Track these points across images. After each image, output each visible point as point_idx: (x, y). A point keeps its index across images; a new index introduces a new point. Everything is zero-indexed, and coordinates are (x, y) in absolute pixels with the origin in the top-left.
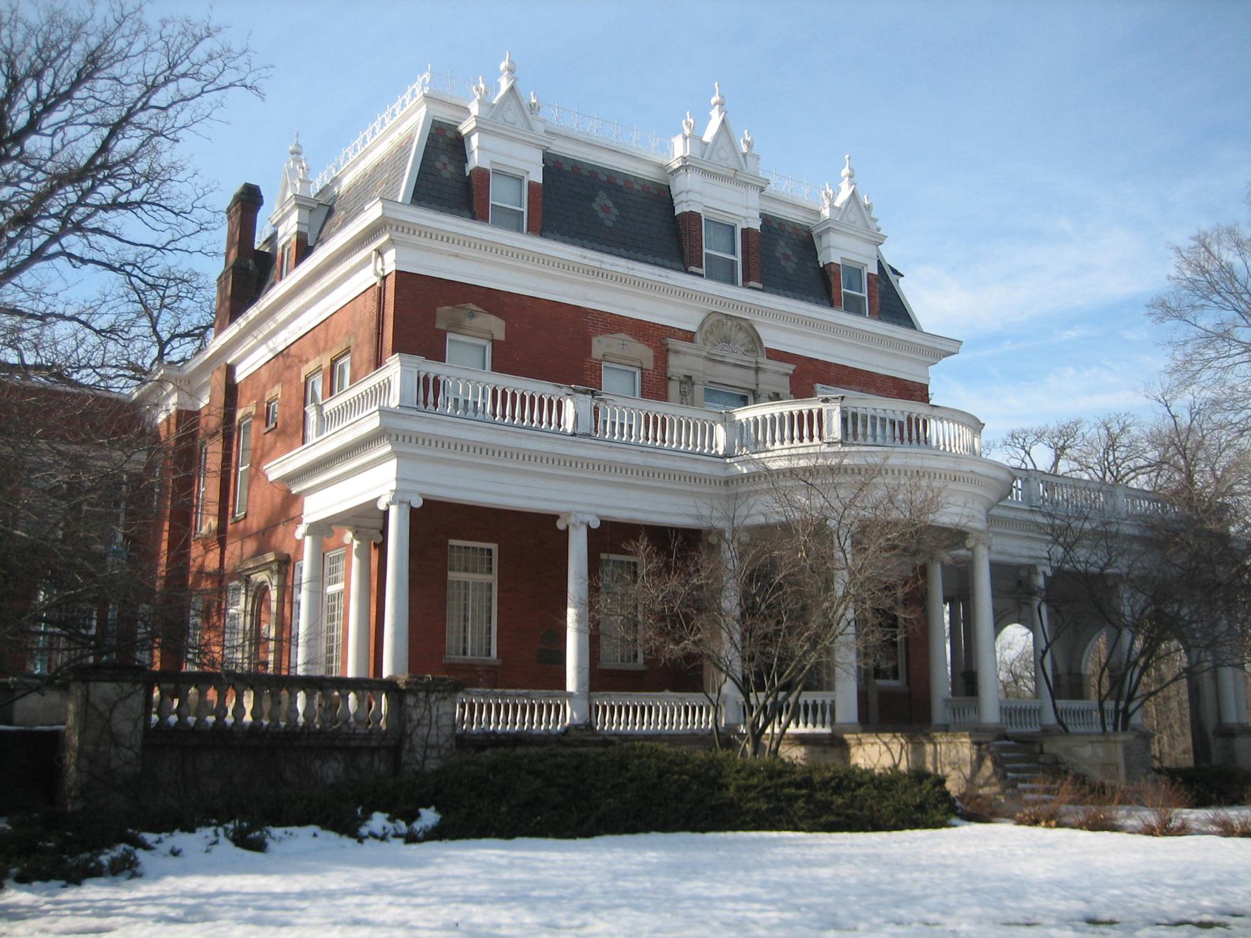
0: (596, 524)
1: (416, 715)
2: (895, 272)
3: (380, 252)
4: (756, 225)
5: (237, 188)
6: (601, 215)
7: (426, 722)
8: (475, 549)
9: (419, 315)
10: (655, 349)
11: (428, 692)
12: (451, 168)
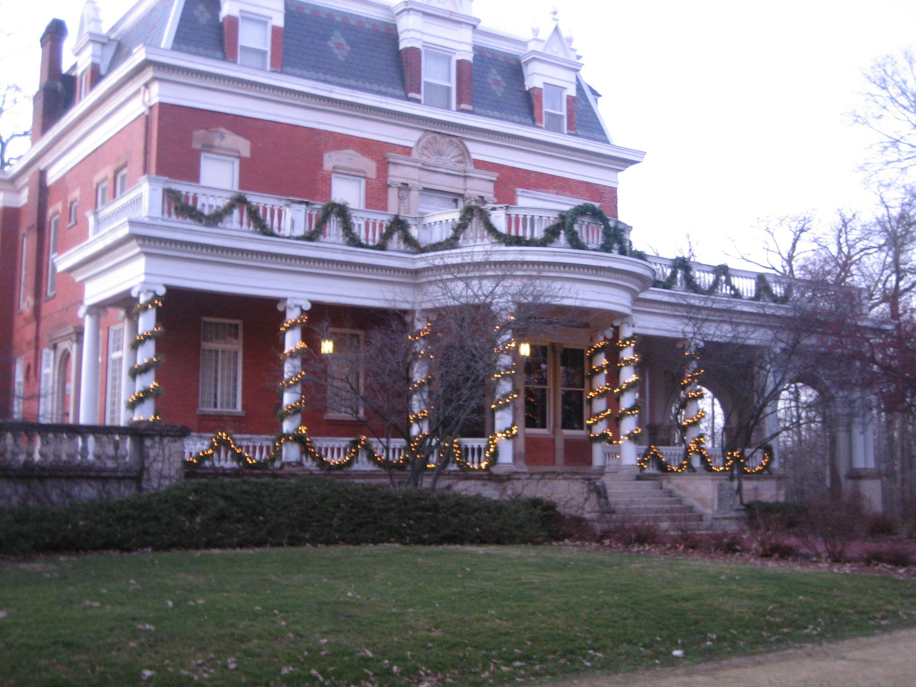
0: (307, 307)
1: (152, 453)
2: (595, 93)
3: (147, 85)
4: (469, 57)
5: (47, 22)
6: (336, 51)
7: (160, 459)
8: (224, 324)
9: (175, 141)
10: (378, 162)
11: (162, 436)
12: (208, 16)
